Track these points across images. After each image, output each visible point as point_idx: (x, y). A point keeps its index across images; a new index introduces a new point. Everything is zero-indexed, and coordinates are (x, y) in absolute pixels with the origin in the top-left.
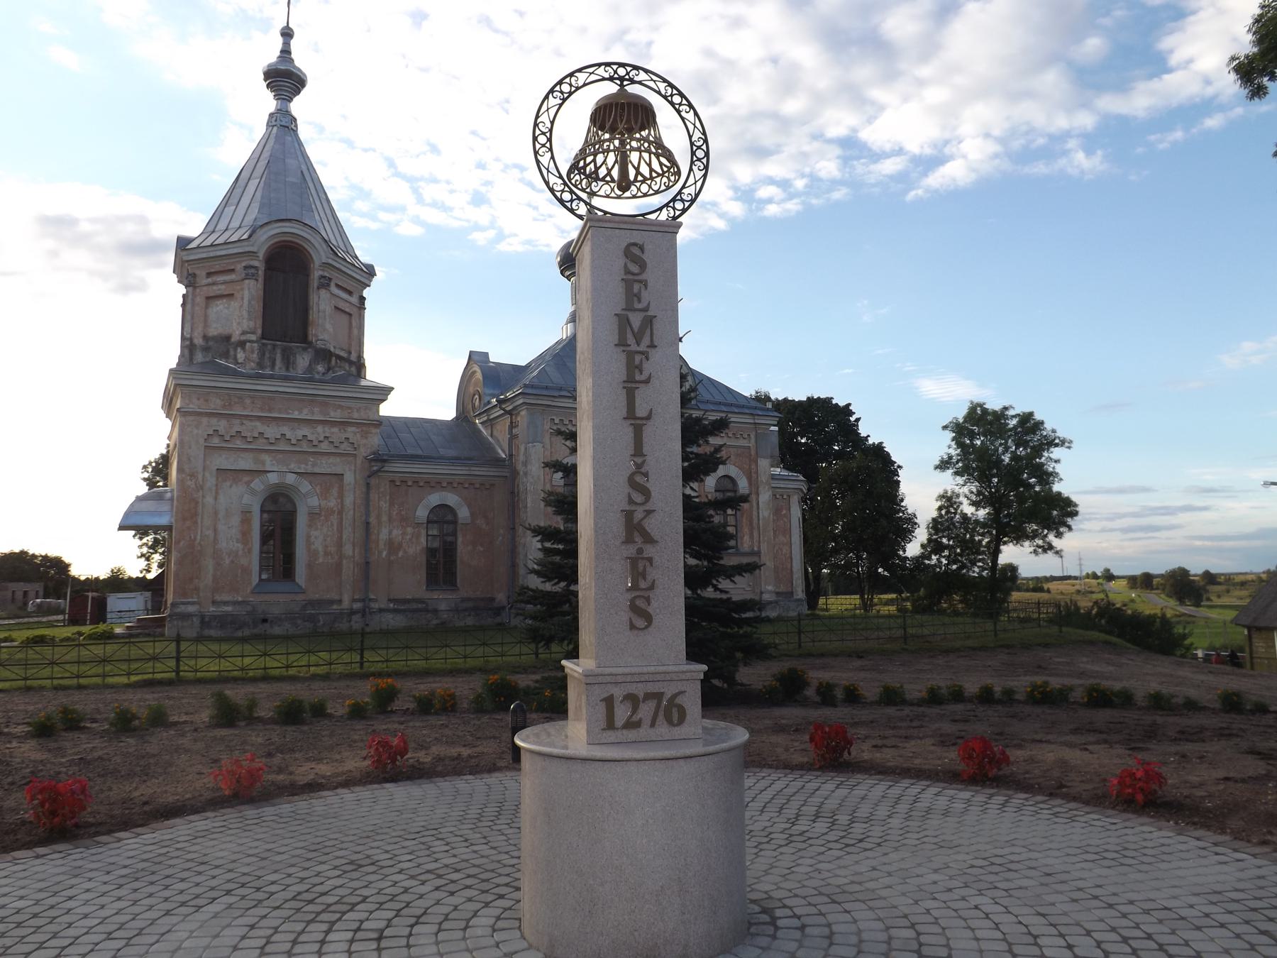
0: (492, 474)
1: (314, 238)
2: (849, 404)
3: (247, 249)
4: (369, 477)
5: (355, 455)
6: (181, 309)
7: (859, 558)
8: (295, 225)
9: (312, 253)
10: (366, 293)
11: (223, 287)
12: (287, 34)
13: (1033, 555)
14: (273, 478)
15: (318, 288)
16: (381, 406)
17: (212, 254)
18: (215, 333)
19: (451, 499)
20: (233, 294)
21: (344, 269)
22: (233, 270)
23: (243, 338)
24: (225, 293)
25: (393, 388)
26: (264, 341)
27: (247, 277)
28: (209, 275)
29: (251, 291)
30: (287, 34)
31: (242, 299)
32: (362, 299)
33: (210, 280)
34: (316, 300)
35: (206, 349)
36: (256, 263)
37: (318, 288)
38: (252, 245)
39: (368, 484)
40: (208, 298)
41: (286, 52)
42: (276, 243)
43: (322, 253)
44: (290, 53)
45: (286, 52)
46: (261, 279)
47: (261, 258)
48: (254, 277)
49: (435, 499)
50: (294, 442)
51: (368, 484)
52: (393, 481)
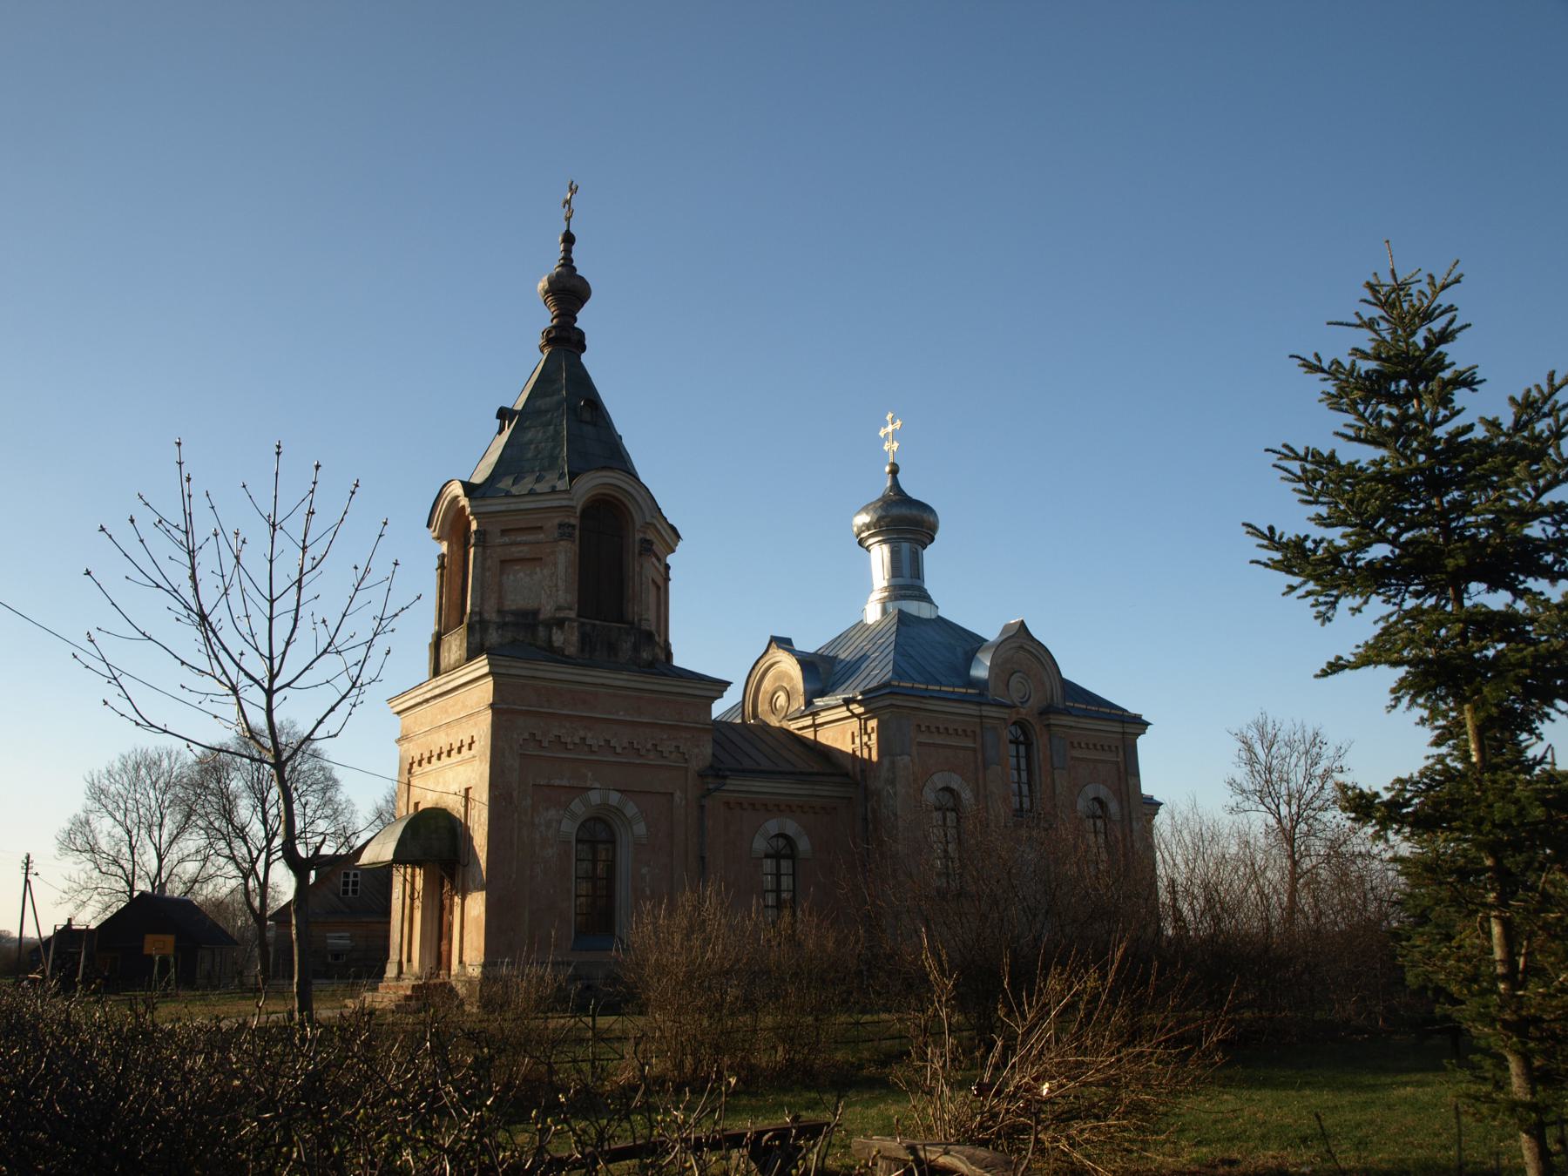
0: (835, 794)
1: (638, 492)
2: (1512, 400)
3: (564, 503)
4: (704, 797)
5: (686, 769)
6: (671, 576)
7: (1196, 929)
8: (617, 476)
9: (632, 509)
10: (670, 559)
11: (525, 548)
12: (569, 239)
13: (1327, 623)
14: (595, 797)
15: (640, 554)
16: (713, 705)
17: (513, 507)
18: (514, 607)
19: (791, 827)
20: (541, 559)
21: (664, 533)
22: (541, 528)
23: (561, 615)
24: (528, 557)
25: (729, 684)
26: (583, 620)
27: (562, 537)
28: (504, 532)
29: (564, 556)
30: (569, 239)
31: (555, 564)
32: (667, 567)
33: (506, 539)
34: (637, 569)
35: (502, 626)
36: (573, 521)
37: (640, 554)
38: (572, 499)
39: (702, 807)
40: (503, 562)
41: (567, 262)
42: (613, 497)
43: (647, 512)
44: (572, 261)
45: (567, 262)
46: (577, 542)
47: (578, 514)
48: (571, 536)
49: (772, 826)
50: (619, 750)
51: (702, 807)
52: (727, 804)
